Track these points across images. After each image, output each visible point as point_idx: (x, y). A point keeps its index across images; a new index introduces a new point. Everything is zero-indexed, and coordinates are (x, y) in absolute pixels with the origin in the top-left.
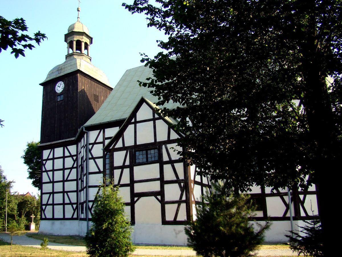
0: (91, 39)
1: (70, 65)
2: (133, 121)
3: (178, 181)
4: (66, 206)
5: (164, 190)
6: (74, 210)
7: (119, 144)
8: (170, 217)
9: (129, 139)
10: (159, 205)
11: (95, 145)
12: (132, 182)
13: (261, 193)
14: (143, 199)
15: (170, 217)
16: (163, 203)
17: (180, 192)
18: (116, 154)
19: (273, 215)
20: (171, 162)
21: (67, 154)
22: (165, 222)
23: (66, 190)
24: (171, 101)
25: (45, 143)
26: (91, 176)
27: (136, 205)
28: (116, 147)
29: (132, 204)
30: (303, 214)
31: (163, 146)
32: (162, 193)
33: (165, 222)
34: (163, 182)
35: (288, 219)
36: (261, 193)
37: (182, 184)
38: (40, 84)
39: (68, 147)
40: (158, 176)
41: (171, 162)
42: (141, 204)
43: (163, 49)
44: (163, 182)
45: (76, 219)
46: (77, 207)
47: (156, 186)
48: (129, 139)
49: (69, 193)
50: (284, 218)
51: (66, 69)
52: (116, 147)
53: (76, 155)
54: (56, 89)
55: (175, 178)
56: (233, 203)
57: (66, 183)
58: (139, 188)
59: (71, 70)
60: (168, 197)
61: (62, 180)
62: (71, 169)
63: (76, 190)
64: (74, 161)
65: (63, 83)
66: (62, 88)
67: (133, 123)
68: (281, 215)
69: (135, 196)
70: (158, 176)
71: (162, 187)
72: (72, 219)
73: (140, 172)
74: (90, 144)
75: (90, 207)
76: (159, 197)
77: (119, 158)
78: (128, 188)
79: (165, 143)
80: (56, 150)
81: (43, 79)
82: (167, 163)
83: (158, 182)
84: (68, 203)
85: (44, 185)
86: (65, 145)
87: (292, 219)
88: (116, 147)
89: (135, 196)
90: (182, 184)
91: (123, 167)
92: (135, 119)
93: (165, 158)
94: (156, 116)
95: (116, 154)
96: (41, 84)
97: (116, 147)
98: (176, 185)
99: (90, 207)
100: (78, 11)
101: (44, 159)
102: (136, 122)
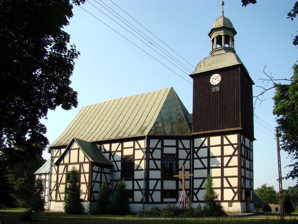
13: (134, 189)
21: (226, 142)
24: (4, 143)
30: (150, 200)
36: (134, 189)
39: (182, 141)
43: (77, 102)
46: (190, 192)
49: (139, 182)
50: (141, 202)
53: (190, 149)
54: (211, 82)
57: (225, 169)
62: (231, 156)
65: (220, 77)
66: (218, 80)
80: (212, 139)
85: (195, 171)
86: (223, 134)
96: (192, 76)
101: (109, 153)
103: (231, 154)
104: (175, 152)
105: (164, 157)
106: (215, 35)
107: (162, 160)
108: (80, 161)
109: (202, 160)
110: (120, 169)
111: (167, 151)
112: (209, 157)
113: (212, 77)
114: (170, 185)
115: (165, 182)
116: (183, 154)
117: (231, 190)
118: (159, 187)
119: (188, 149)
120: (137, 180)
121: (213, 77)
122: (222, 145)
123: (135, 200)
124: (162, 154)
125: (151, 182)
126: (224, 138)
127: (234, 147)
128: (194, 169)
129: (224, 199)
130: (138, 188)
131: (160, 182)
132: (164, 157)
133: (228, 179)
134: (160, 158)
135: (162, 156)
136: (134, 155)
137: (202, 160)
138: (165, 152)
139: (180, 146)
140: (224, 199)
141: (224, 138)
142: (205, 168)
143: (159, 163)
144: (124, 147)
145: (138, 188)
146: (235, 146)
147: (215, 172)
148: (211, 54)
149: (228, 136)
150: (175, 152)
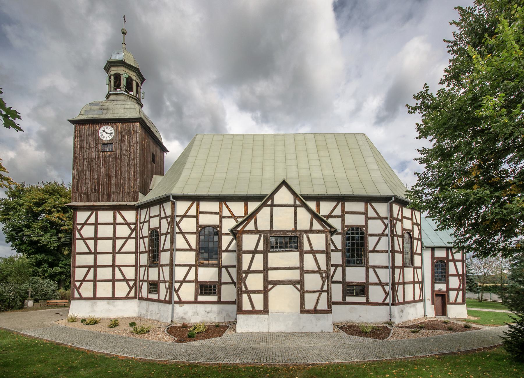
0: (143, 80)
1: (123, 106)
2: (269, 203)
3: (318, 271)
4: (117, 283)
5: (304, 279)
6: (131, 289)
7: (251, 226)
8: (309, 306)
9: (263, 221)
10: (298, 293)
11: (184, 219)
12: (266, 269)
14: (278, 287)
15: (309, 306)
16: (303, 292)
17: (321, 283)
18: (245, 237)
19: (372, 301)
20: (313, 252)
22: (303, 311)
23: (117, 263)
25: (88, 202)
26: (177, 253)
27: (270, 293)
28: (246, 229)
29: (265, 292)
31: (305, 235)
32: (301, 282)
33: (303, 311)
34: (303, 271)
35: (387, 304)
37: (324, 275)
38: (68, 120)
40: (298, 265)
41: (313, 252)
42: (274, 293)
44: (303, 271)
45: (135, 298)
47: (295, 275)
48: (263, 221)
50: (383, 304)
51: (116, 111)
52: (245, 229)
54: (100, 134)
55: (316, 269)
56: (22, 242)
58: (273, 276)
59: (126, 114)
60: (308, 286)
61: (111, 251)
63: (134, 264)
64: (132, 231)
67: (268, 206)
68: (381, 301)
69: (269, 284)
70: (298, 265)
71: (302, 276)
72: (127, 298)
73: (276, 259)
74: (177, 216)
75: (177, 289)
76: (298, 286)
77: (249, 242)
78: (261, 275)
79: (306, 232)
81: (366, 134)
82: (308, 252)
83: (298, 271)
84: (324, 310)
87: (390, 304)
88: (246, 229)
89: (269, 284)
90: (324, 275)
91: (255, 252)
92: (272, 202)
93: (306, 247)
94: (298, 203)
95: (245, 237)
97: (245, 229)
98: (318, 275)
99: (177, 289)
100: (124, 33)
102: (272, 206)
103: (127, 235)
104: (217, 223)
105: (201, 229)
106: (114, 70)
107: (198, 233)
108: (346, 215)
109: (87, 241)
110: (194, 247)
111: (205, 220)
112: (96, 239)
113: (102, 129)
114: (356, 274)
115: (202, 271)
116: (375, 227)
117: (125, 283)
118: (191, 276)
119: (133, 224)
120: (374, 267)
121: (104, 128)
122: (115, 224)
123: (371, 300)
124: (198, 225)
125: (177, 269)
126: (118, 215)
127: (130, 228)
128: (136, 253)
129: (97, 296)
130: (456, 273)
131: (193, 269)
132: (201, 229)
133: (122, 268)
134: (194, 230)
135: (197, 229)
136: (220, 225)
137: (87, 241)
138: (201, 222)
139: (226, 213)
140: (97, 296)
141: (118, 215)
142: (90, 253)
143: (192, 239)
144: (346, 210)
145: (456, 273)
146: (133, 227)
147: (105, 260)
148: (108, 96)
149: (123, 213)
150: (217, 223)
